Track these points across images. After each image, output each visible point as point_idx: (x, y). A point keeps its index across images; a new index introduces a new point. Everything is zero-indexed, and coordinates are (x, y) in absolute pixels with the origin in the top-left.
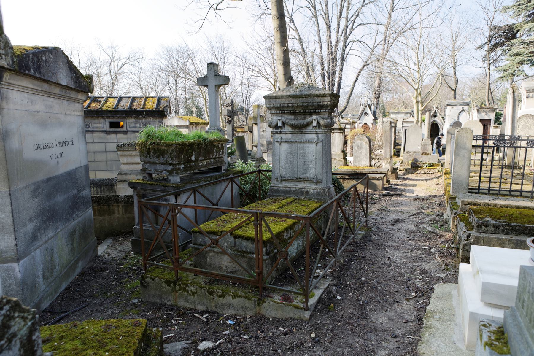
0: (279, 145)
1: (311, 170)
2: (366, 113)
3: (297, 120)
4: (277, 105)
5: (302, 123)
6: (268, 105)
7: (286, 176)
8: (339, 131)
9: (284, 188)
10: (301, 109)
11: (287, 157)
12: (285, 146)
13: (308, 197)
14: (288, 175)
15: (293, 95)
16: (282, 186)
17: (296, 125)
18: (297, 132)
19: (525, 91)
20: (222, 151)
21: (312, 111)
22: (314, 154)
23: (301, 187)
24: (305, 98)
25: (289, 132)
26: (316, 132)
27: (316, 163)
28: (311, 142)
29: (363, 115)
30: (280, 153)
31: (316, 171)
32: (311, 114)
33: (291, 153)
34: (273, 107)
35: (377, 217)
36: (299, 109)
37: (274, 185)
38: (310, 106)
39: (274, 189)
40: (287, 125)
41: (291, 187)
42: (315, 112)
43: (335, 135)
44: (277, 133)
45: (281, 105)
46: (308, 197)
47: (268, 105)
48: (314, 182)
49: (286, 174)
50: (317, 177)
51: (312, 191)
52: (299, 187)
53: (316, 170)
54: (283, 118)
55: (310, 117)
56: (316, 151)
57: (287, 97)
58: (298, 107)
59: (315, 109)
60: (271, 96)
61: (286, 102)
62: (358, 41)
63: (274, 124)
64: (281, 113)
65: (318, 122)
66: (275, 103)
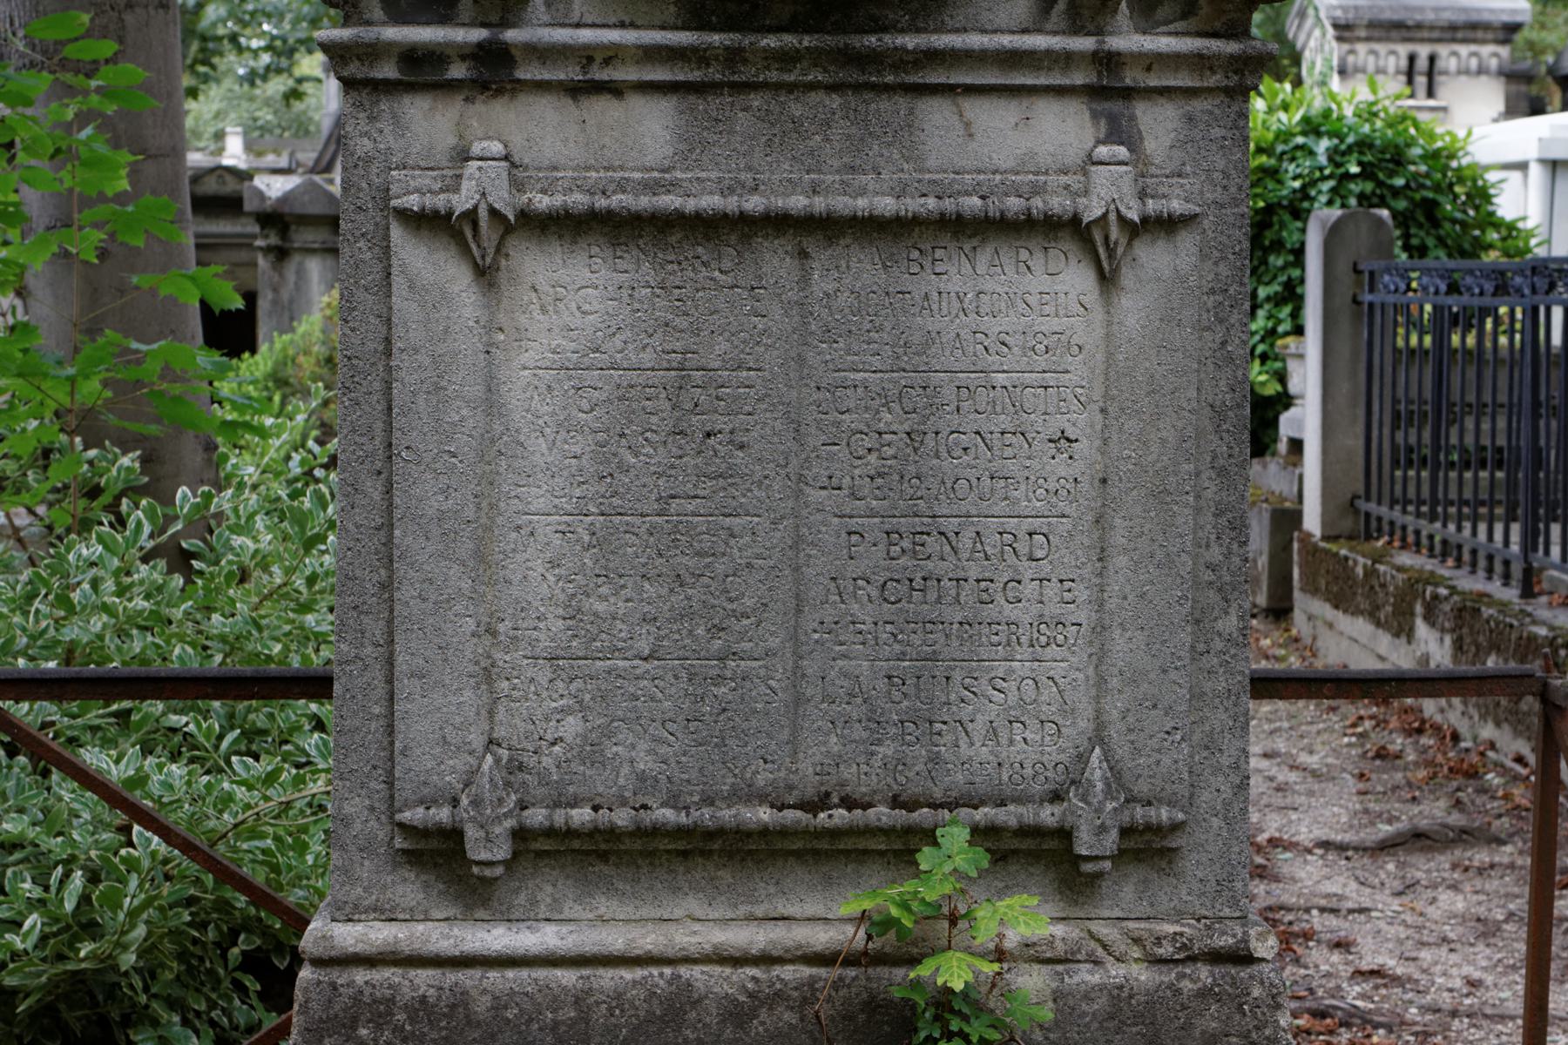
18: (787, 58)
19: (1331, 32)
22: (1079, 422)
26: (1108, 61)
49: (591, 751)
53: (1100, 657)
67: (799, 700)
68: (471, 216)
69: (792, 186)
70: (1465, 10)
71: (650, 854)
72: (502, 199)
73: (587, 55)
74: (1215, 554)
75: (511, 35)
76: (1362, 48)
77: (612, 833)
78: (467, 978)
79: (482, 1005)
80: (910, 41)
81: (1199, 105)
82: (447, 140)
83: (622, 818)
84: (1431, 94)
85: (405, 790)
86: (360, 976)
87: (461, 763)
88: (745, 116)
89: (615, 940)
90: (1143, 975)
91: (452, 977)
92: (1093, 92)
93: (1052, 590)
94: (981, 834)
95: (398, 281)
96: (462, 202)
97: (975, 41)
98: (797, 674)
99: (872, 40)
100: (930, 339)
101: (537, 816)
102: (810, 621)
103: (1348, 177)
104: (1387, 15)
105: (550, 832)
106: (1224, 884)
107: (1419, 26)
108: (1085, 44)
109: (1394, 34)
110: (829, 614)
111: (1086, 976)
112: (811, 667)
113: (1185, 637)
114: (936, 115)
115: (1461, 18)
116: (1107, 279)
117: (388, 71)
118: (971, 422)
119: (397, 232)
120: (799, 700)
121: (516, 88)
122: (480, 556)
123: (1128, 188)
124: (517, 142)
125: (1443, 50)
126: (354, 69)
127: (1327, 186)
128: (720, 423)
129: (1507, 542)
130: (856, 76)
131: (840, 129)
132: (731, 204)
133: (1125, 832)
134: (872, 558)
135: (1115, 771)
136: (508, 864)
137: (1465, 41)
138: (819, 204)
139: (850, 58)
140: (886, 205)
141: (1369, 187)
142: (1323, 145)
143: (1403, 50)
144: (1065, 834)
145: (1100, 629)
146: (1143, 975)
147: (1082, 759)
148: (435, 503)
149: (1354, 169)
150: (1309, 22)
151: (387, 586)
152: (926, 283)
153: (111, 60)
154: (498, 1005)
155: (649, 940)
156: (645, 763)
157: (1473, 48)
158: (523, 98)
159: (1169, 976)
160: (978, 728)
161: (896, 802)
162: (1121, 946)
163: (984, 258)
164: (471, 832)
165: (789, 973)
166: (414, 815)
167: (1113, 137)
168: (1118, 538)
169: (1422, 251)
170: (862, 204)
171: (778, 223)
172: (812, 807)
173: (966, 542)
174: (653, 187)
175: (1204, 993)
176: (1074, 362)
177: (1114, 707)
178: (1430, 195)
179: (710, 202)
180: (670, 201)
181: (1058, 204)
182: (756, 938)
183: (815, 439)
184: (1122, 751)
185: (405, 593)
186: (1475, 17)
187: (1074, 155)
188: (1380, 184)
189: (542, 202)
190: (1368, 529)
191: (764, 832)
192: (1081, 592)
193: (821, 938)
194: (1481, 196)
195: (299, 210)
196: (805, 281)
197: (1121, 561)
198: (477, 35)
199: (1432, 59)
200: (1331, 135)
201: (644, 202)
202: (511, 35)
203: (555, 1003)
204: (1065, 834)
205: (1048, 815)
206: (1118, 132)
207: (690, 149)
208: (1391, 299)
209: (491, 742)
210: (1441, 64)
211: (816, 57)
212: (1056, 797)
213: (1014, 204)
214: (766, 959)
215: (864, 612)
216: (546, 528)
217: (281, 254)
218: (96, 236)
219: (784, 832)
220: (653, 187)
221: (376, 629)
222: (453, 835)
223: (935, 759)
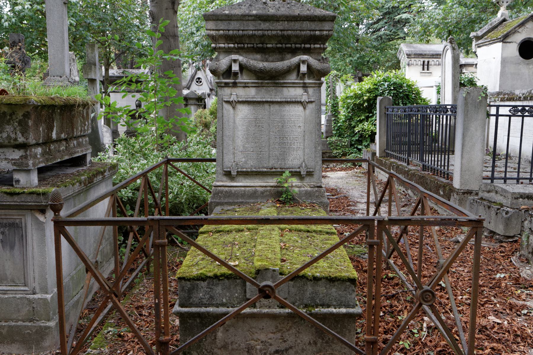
2: (199, 78)
12: (244, 111)
14: (251, 165)
18: (268, 83)
19: (406, 56)
20: (87, 123)
21: (297, 46)
22: (301, 124)
25: (253, 83)
26: (304, 83)
29: (195, 81)
32: (294, 52)
33: (256, 123)
34: (221, 36)
35: (325, 246)
42: (304, 47)
44: (227, 85)
45: (241, 32)
49: (246, 162)
50: (306, 166)
53: (304, 152)
57: (253, 18)
58: (271, 37)
61: (251, 28)
63: (222, 69)
66: (226, 28)
67: (269, 157)
68: (232, 101)
69: (269, 98)
70: (436, 51)
71: (252, 175)
72: (236, 99)
73: (245, 83)
74: (318, 140)
75: (237, 81)
76: (413, 60)
77: (248, 172)
78: (232, 188)
79: (233, 191)
80: (282, 81)
81: (315, 88)
82: (229, 93)
83: (249, 170)
84: (428, 70)
85: (225, 167)
86: (219, 188)
87: (231, 164)
88: (263, 90)
89: (248, 184)
90: (309, 189)
91: (230, 188)
92: (303, 87)
93: (298, 144)
94: (290, 172)
95: (224, 109)
96: (231, 100)
97: (289, 81)
98: (269, 154)
99: (278, 81)
100: (284, 115)
101: (239, 170)
102: (271, 148)
103: (391, 90)
104: (418, 52)
105: (241, 172)
106: (319, 179)
107: (425, 55)
108: (302, 81)
109: (420, 56)
110: (273, 147)
111: (303, 189)
112: (271, 153)
113: (314, 149)
114: (285, 90)
115: (435, 53)
116: (305, 108)
117: (223, 85)
118: (289, 125)
119: (224, 103)
120: (269, 157)
121: (237, 87)
122: (233, 140)
123: (307, 98)
124: (237, 93)
125: (431, 60)
126: (219, 85)
127: (387, 92)
128: (261, 125)
129: (434, 165)
130: (276, 85)
131: (274, 91)
132: (262, 100)
133: (307, 172)
134: (278, 140)
135: (306, 166)
136: (236, 175)
137: (435, 58)
138: (271, 100)
139: (275, 83)
140: (279, 100)
141: (395, 92)
142: (386, 84)
143: (422, 60)
144: (300, 172)
145: (304, 149)
146: (309, 189)
147: (302, 163)
148: (228, 134)
149: (392, 88)
150: (402, 54)
151: (222, 143)
152: (284, 109)
153: (175, 77)
154: (235, 192)
155: (252, 184)
156: (252, 164)
157: (437, 59)
158: (238, 88)
159: (312, 189)
160: (290, 160)
161: (280, 168)
162: (307, 185)
163: (290, 106)
164: (232, 171)
165: (268, 188)
166: (225, 170)
167: (305, 92)
168: (306, 138)
169: (406, 104)
170: (276, 100)
171: (267, 102)
172: (271, 169)
173: (288, 138)
174: (253, 98)
175: (316, 191)
176: (301, 118)
177: (306, 158)
178: (407, 93)
179: (259, 100)
180: (255, 100)
181: (299, 100)
182: (265, 184)
183: (271, 127)
184: (307, 163)
185: (225, 144)
186: (438, 53)
187: (301, 94)
188: (397, 91)
189: (240, 100)
190: (388, 155)
191: (265, 172)
192: (302, 144)
193: (272, 184)
194: (418, 93)
195: (190, 97)
196: (270, 108)
197: (306, 141)
198: (233, 81)
199: (428, 62)
200: (388, 82)
201: (252, 100)
202: (237, 81)
203: (242, 191)
204: (300, 172)
205: (298, 170)
206: (306, 91)
207: (257, 93)
208: (415, 113)
209: (234, 161)
210: (430, 63)
211: (271, 83)
212: (299, 168)
213: (294, 100)
214: (266, 187)
215: (277, 147)
216: (241, 137)
217: (186, 105)
218: (171, 103)
219: (268, 172)
220: (253, 98)
221: (221, 148)
222: (230, 172)
223: (285, 164)
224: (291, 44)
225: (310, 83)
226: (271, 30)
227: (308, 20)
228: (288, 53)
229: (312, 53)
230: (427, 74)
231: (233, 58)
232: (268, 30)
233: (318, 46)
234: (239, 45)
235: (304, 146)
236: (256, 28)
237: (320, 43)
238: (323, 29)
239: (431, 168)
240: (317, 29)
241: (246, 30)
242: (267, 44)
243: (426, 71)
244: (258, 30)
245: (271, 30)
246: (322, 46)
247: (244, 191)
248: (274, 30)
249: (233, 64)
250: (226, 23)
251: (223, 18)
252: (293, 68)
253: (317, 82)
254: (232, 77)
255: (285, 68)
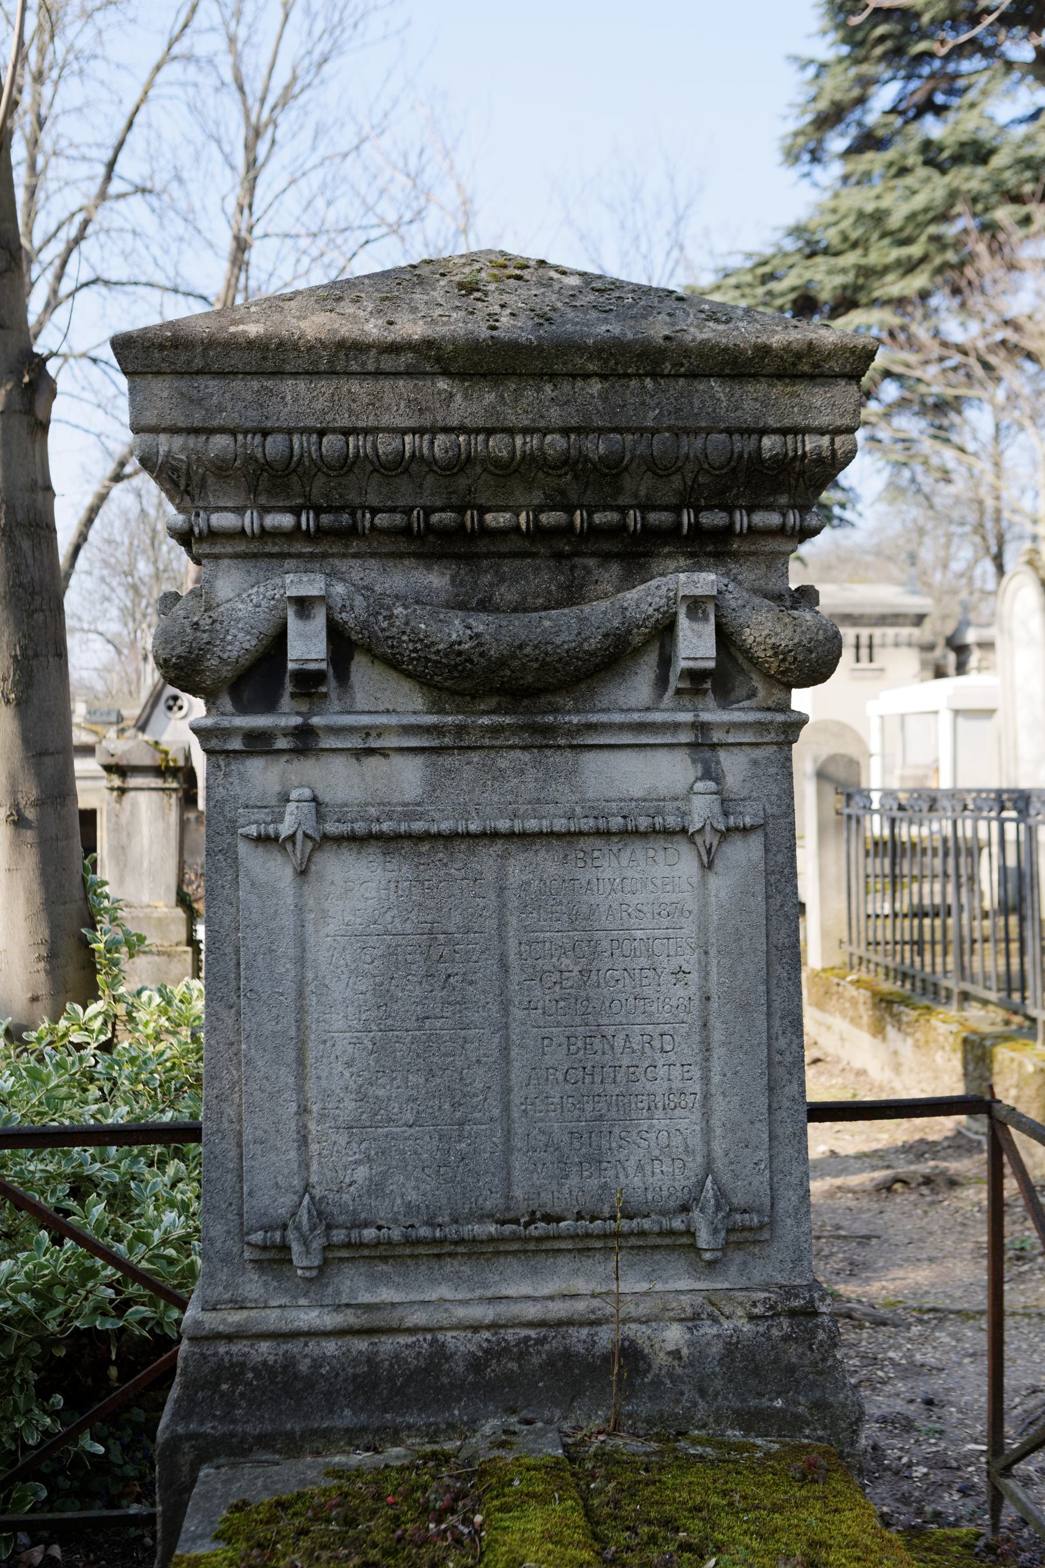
0: (288, 873)
1: (660, 1122)
3: (485, 606)
4: (275, 445)
5: (566, 639)
6: (164, 443)
7: (383, 1210)
8: (158, 783)
9: (361, 1345)
10: (537, 498)
11: (384, 999)
13: (644, 1408)
15: (474, 347)
16: (330, 1320)
17: (503, 662)
18: (496, 730)
21: (655, 518)
22: (690, 960)
23: (559, 1309)
24: (596, 387)
25: (408, 730)
26: (701, 727)
27: (707, 1048)
28: (629, 834)
29: (161, 706)
30: (301, 961)
31: (707, 1132)
34: (222, 469)
36: (520, 497)
37: (236, 1317)
38: (653, 466)
39: (235, 1370)
40: (393, 663)
41: (440, 1317)
42: (696, 528)
43: (134, 805)
45: (331, 443)
46: (644, 1408)
47: (164, 443)
48: (704, 1239)
49: (376, 1187)
50: (721, 1194)
51: (674, 1335)
52: (532, 1311)
53: (707, 1116)
54: (340, 589)
55: (627, 582)
56: (703, 928)
59: (688, 499)
60: (210, 344)
62: (84, 355)
63: (233, 652)
64: (320, 534)
65: (725, 638)
66: (252, 418)
73: (367, 732)
75: (315, 720)
80: (575, 719)
81: (759, 753)
84: (871, 660)
90: (747, 1328)
93: (676, 1072)
96: (285, 829)
108: (686, 717)
117: (236, 744)
130: (539, 740)
135: (721, 1194)
145: (707, 1096)
147: (701, 1184)
156: (412, 1196)
173: (619, 1042)
184: (726, 1178)
198: (297, 720)
203: (355, 1362)
210: (877, 641)
224: (623, 510)
225: (730, 727)
226: (511, 431)
227: (720, 376)
228: (606, 557)
229: (735, 556)
230: (869, 674)
231: (293, 592)
232: (490, 432)
233: (774, 519)
234: (326, 519)
235: (706, 1080)
236: (427, 421)
237: (783, 500)
238: (800, 421)
239: (923, 981)
240: (772, 422)
241: (366, 431)
242: (483, 510)
243: (864, 664)
244: (433, 431)
245: (511, 431)
246: (792, 518)
247: (371, 1360)
248: (526, 431)
249: (293, 624)
250: (247, 388)
251: (235, 360)
252: (636, 640)
253: (767, 716)
254: (286, 702)
255: (593, 644)
